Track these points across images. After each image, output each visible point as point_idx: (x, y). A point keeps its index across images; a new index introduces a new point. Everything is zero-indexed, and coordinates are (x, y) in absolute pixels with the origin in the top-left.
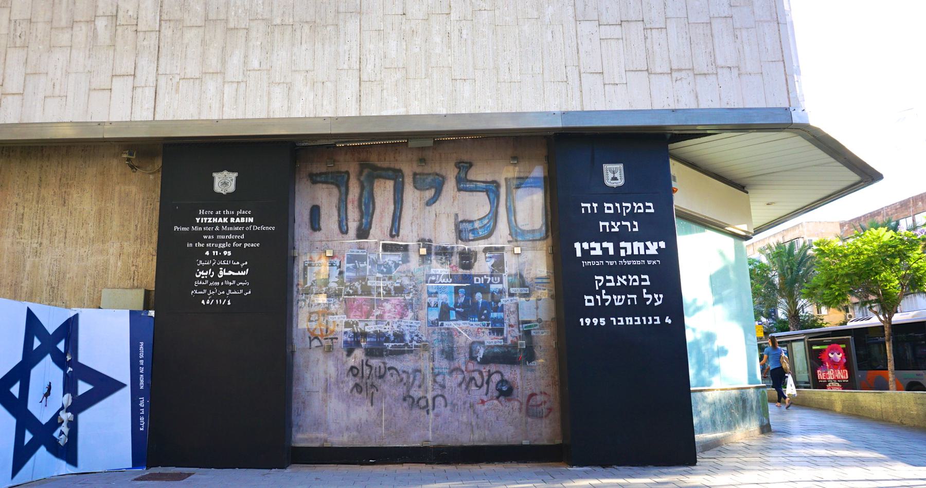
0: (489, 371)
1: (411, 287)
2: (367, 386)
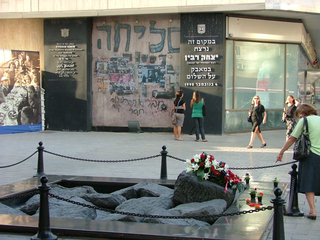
0: (159, 101)
1: (133, 70)
2: (117, 106)
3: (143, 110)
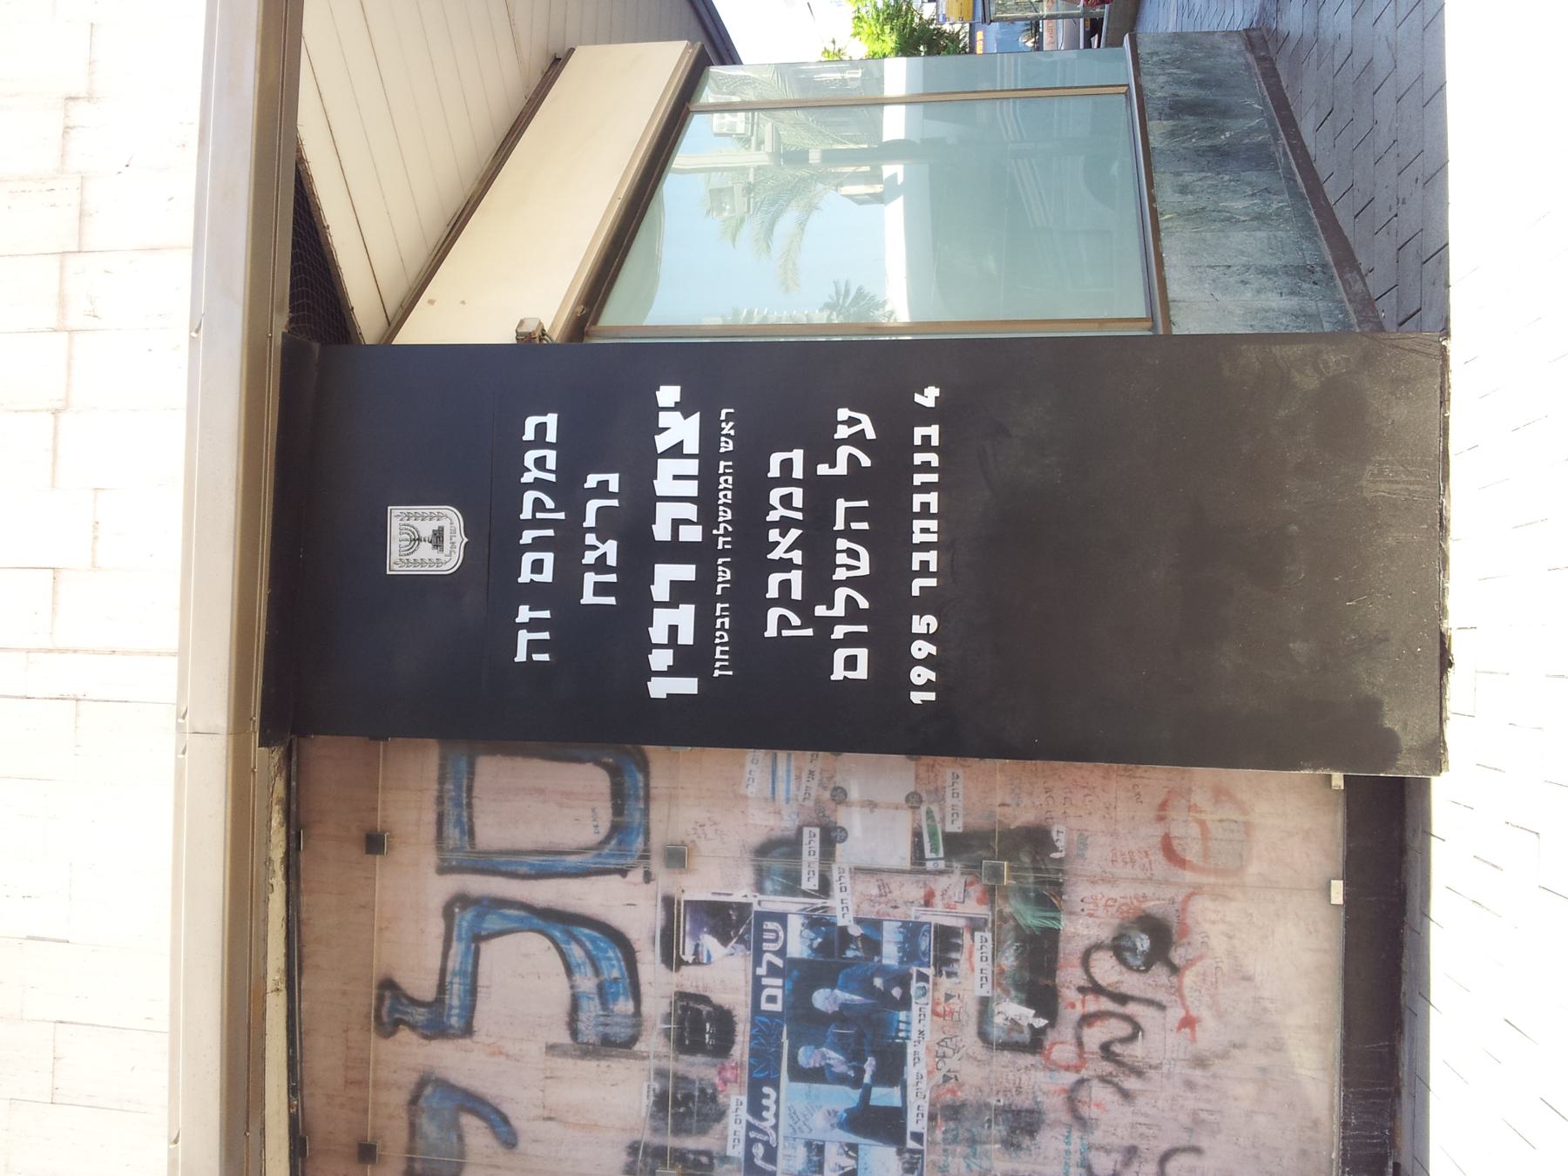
0: (1081, 990)
3: (1165, 1158)
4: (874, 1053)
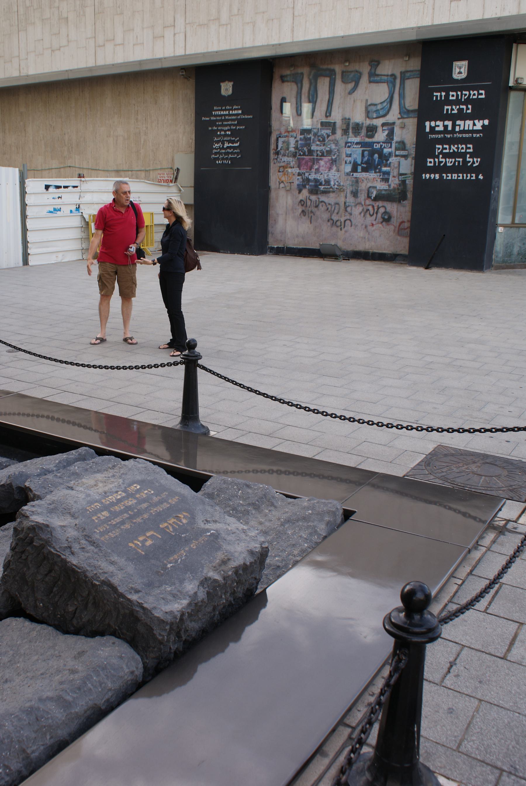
0: (378, 206)
1: (336, 150)
3: (350, 220)
4: (367, 166)
